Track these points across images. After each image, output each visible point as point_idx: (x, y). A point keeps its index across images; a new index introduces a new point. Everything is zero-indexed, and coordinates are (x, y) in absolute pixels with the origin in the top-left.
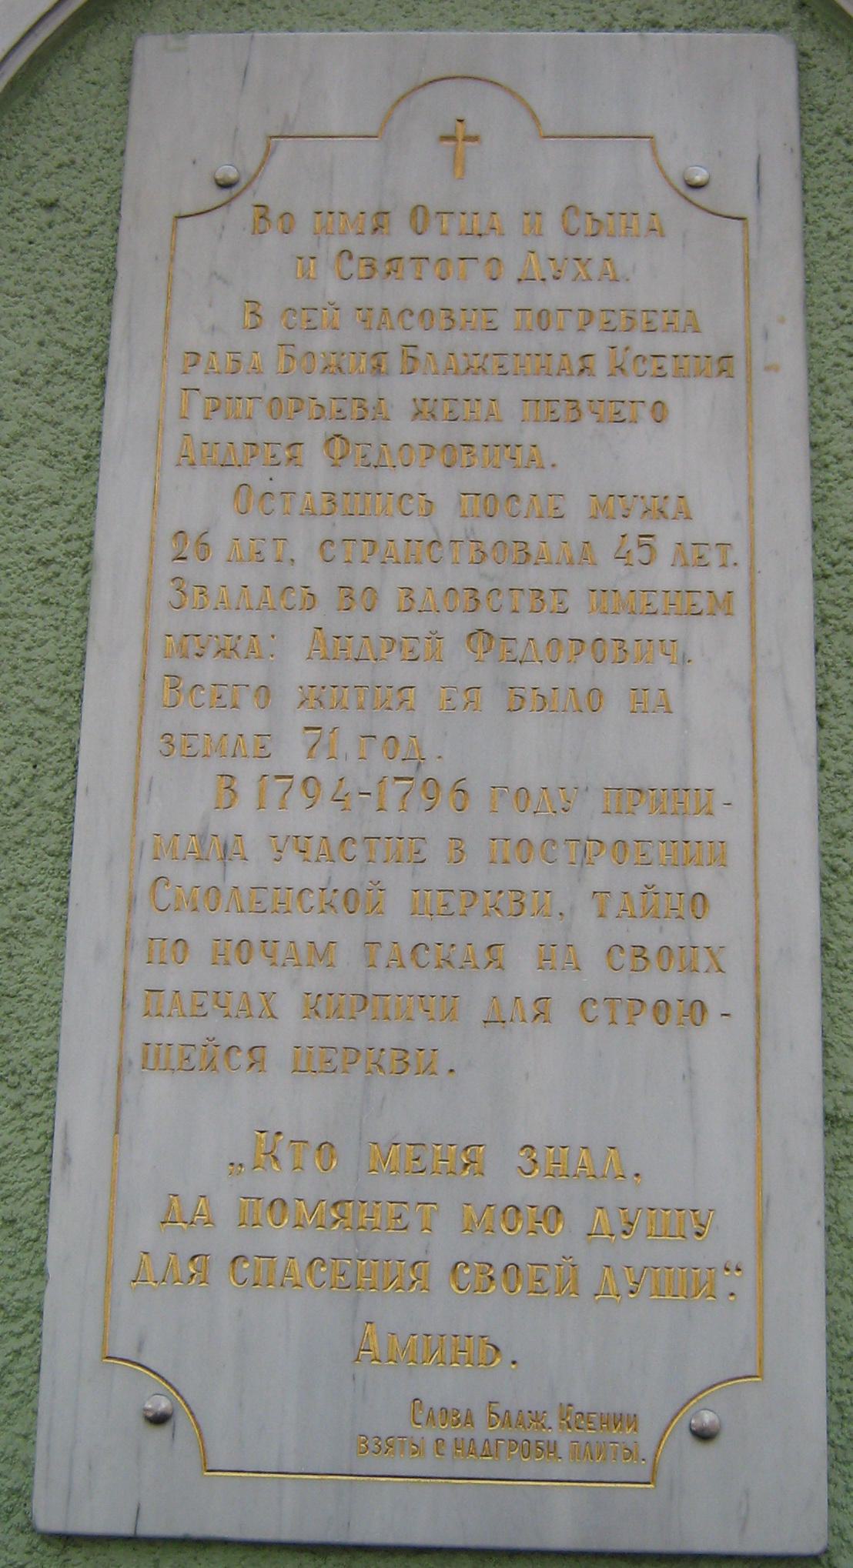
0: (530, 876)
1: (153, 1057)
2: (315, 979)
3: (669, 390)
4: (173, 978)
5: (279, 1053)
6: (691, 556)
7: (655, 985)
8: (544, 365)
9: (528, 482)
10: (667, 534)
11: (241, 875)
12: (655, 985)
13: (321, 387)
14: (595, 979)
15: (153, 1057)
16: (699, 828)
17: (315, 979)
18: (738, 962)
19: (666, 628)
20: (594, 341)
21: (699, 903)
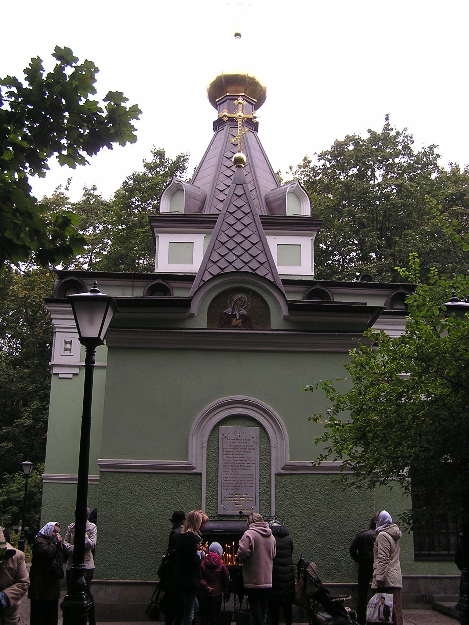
0: (244, 479)
1: (223, 489)
2: (232, 485)
3: (251, 450)
4: (224, 485)
5: (230, 489)
6: (252, 461)
7: (251, 485)
8: (244, 449)
9: (243, 456)
10: (251, 459)
11: (228, 479)
12: (251, 485)
13: (231, 450)
14: (247, 485)
15: (223, 489)
16: (253, 476)
17: (232, 485)
18: (255, 484)
19: (251, 465)
20: (247, 447)
21: (253, 481)
